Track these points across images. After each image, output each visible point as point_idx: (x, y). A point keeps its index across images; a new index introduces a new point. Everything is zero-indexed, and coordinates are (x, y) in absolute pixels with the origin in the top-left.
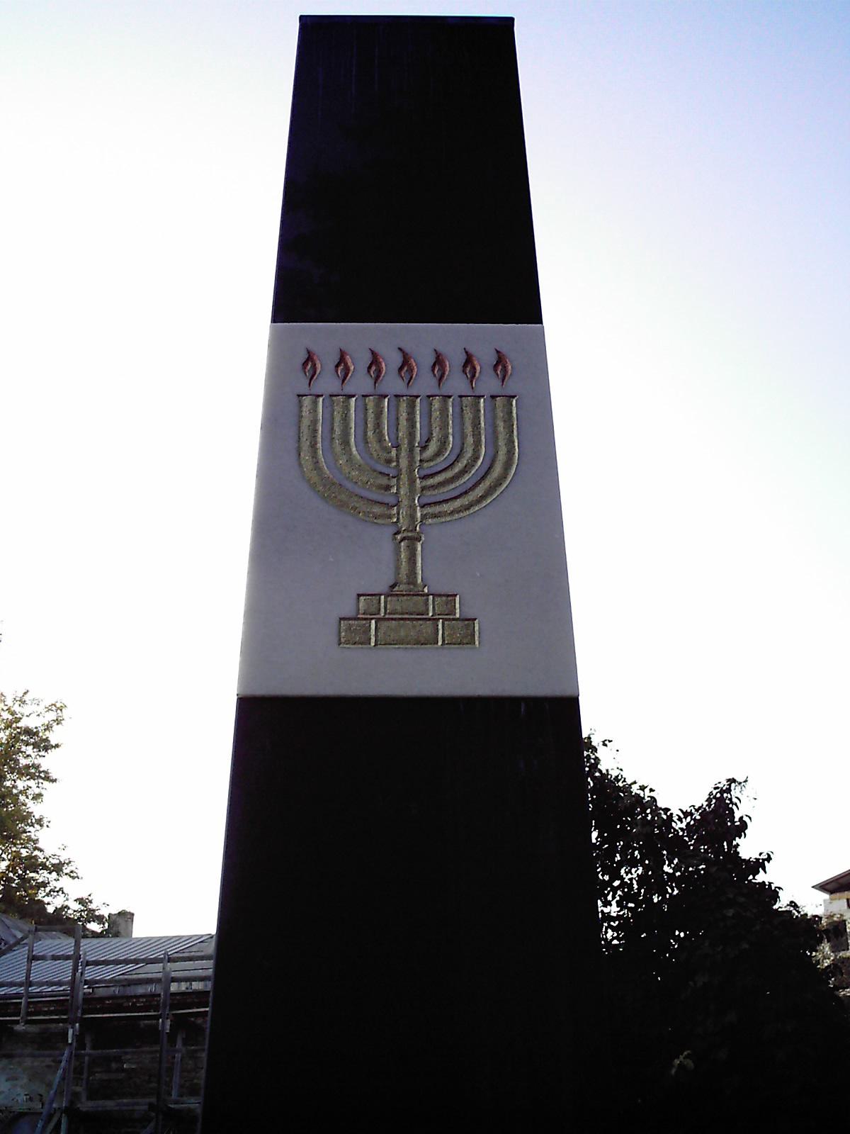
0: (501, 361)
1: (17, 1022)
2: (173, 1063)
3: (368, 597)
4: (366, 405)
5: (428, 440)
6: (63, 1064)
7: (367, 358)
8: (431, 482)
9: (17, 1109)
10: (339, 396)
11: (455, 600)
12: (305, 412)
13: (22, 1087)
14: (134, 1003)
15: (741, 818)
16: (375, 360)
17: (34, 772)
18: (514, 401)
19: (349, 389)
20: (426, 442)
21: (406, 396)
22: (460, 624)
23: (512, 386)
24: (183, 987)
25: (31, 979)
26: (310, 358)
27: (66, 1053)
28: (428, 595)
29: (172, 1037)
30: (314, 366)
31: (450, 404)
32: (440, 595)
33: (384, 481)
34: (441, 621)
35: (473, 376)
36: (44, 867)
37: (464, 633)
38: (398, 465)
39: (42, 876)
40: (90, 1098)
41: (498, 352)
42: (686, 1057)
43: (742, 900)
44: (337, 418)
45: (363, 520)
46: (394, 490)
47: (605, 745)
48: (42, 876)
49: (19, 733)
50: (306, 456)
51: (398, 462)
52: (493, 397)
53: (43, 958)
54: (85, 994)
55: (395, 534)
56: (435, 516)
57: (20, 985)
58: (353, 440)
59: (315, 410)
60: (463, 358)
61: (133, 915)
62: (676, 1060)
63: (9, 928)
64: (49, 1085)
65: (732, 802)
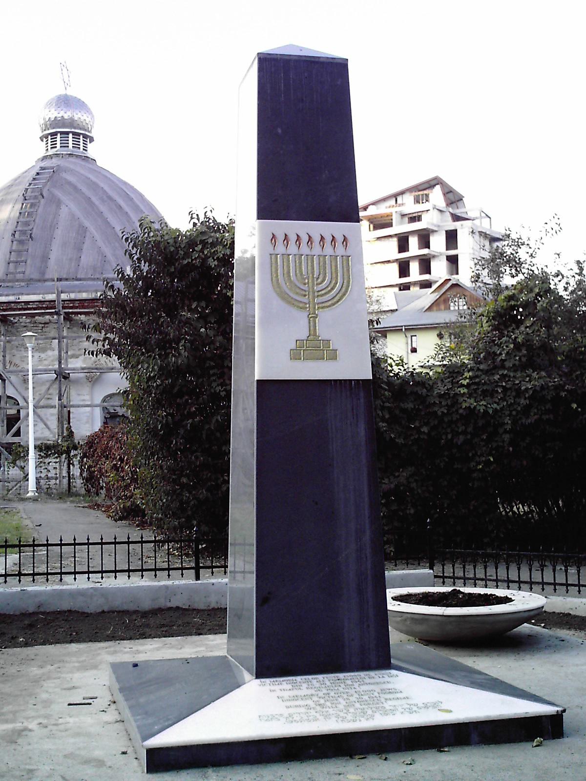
30: (275, 241)
33: (304, 293)
37: (333, 356)
46: (307, 297)
52: (342, 256)
56: (323, 308)
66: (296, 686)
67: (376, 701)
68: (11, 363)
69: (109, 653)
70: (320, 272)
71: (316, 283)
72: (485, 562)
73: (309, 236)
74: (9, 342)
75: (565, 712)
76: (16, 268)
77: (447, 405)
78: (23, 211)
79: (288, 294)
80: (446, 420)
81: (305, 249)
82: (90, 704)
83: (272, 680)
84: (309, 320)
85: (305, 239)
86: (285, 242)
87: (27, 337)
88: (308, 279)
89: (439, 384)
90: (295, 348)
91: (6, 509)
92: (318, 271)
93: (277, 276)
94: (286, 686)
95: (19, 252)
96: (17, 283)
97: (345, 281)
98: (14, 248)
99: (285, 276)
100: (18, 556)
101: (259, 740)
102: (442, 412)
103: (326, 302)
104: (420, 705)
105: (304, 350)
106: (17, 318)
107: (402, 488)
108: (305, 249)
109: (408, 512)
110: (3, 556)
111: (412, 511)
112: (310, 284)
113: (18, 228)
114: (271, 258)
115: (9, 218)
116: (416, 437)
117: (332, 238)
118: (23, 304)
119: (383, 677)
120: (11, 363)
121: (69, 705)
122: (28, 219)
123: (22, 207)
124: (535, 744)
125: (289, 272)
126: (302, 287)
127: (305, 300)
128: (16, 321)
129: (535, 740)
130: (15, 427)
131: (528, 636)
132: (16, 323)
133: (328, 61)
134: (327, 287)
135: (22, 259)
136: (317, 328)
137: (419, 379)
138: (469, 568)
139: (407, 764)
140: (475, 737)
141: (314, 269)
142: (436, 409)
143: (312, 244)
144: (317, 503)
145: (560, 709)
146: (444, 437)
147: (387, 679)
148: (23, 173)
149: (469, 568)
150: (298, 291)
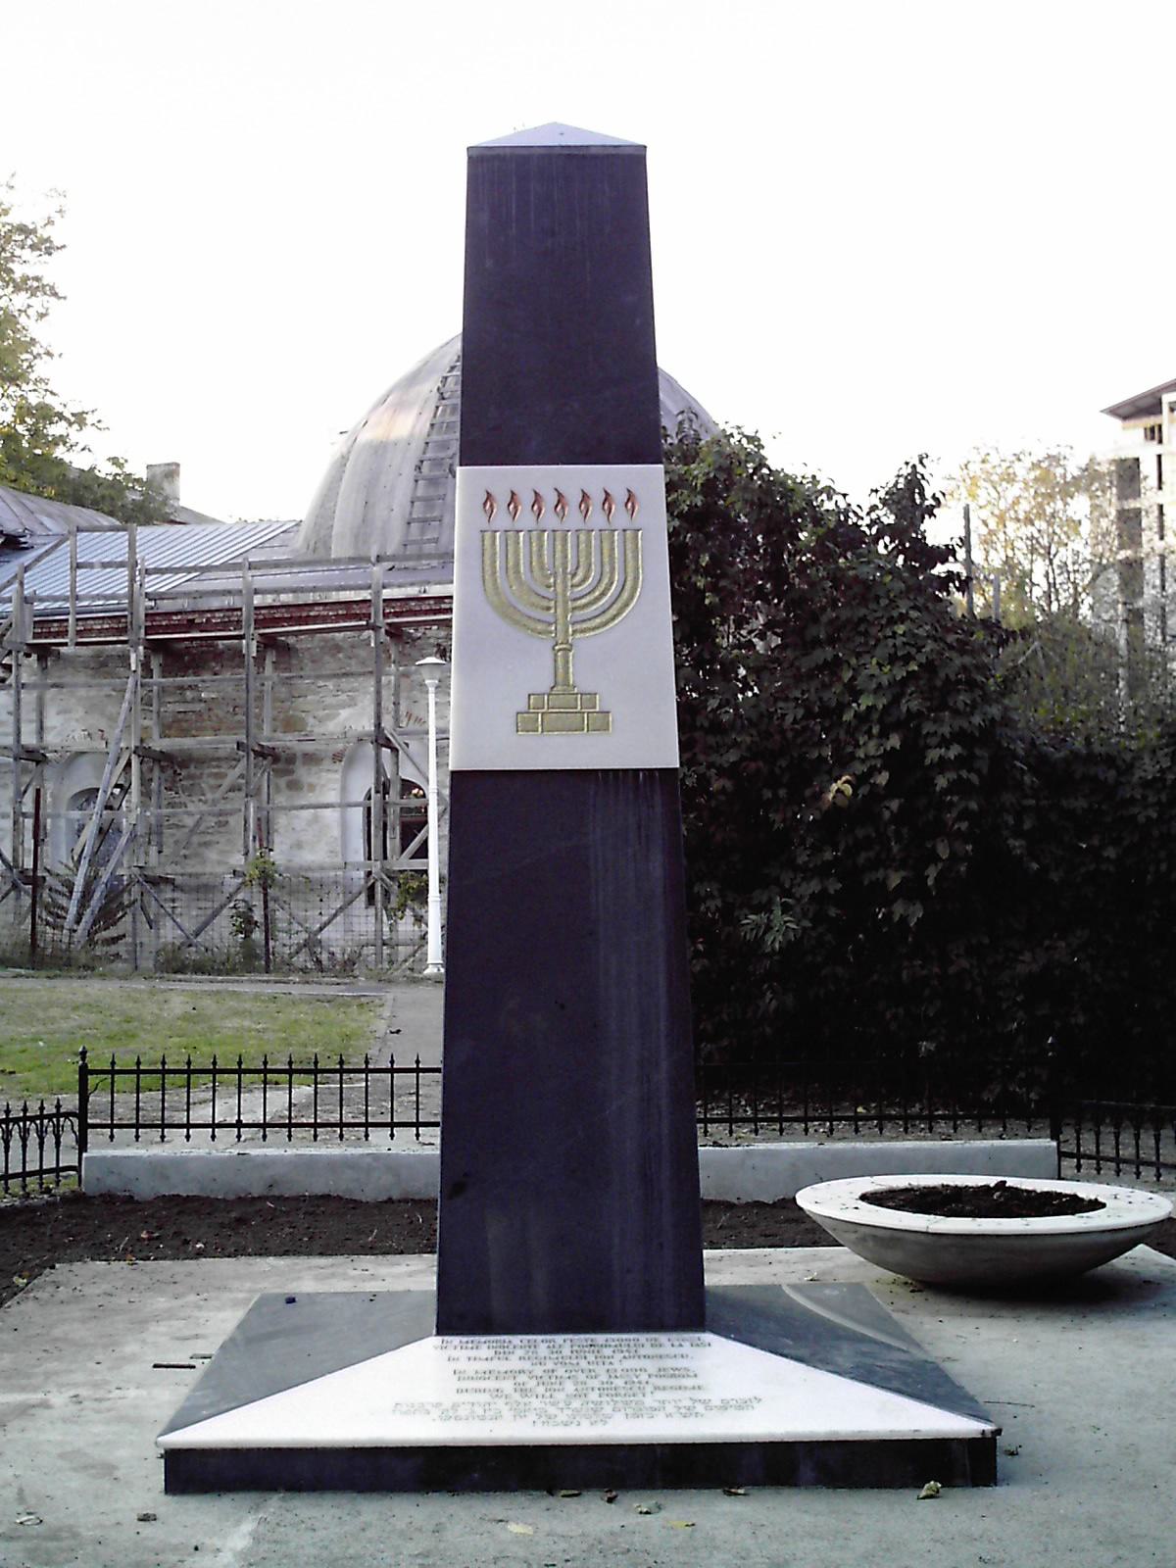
0: (631, 497)
1: (66, 644)
2: (261, 692)
5: (577, 568)
6: (128, 695)
8: (579, 603)
9: (75, 748)
12: (487, 542)
13: (77, 720)
14: (208, 620)
17: (31, 286)
24: (269, 600)
25: (26, 592)
27: (131, 681)
29: (260, 661)
30: (491, 506)
33: (545, 603)
36: (61, 416)
37: (601, 723)
39: (56, 429)
40: (163, 735)
41: (629, 491)
42: (845, 782)
43: (914, 614)
46: (552, 611)
49: (10, 231)
52: (624, 530)
53: (91, 566)
54: (146, 609)
56: (583, 631)
57: (66, 599)
61: (178, 465)
64: (113, 719)
65: (923, 478)
66: (503, 1354)
67: (635, 1390)
68: (409, 716)
69: (317, 1278)
70: (578, 562)
71: (569, 584)
72: (1137, 1128)
73: (560, 495)
74: (406, 675)
75: (1000, 1434)
76: (423, 532)
77: (1159, 803)
78: (436, 421)
79: (515, 608)
80: (1156, 833)
81: (550, 519)
82: (193, 1367)
83: (464, 1339)
84: (556, 655)
85: (550, 499)
86: (512, 506)
87: (426, 669)
88: (555, 577)
89: (1147, 760)
90: (526, 709)
91: (362, 999)
92: (575, 560)
93: (494, 573)
94: (485, 1352)
95: (428, 501)
96: (424, 562)
97: (629, 578)
98: (420, 493)
99: (511, 572)
100: (311, 1090)
101: (372, 1448)
102: (1149, 818)
103: (590, 619)
104: (716, 1402)
105: (543, 714)
106: (422, 629)
107: (1057, 972)
108: (550, 519)
109: (1073, 1021)
110: (283, 1089)
111: (1081, 1020)
112: (559, 588)
113: (429, 455)
114: (483, 537)
115: (412, 435)
116: (1092, 867)
117: (604, 496)
118: (432, 602)
119: (681, 1345)
120: (409, 716)
121: (155, 1366)
122: (446, 437)
123: (435, 414)
124: (923, 1493)
125: (517, 564)
126: (543, 591)
127: (548, 616)
128: (419, 635)
129: (927, 1486)
130: (417, 839)
131: (1145, 1282)
132: (419, 638)
133: (606, 152)
134: (593, 591)
135: (434, 515)
136: (571, 670)
137: (1103, 750)
138: (1147, 1140)
139: (641, 1513)
140: (806, 1471)
141: (566, 557)
142: (1135, 810)
143: (563, 508)
144: (562, 1007)
145: (988, 1427)
146: (1152, 869)
147: (687, 1349)
148: (442, 347)
149: (1127, 1138)
150: (535, 599)
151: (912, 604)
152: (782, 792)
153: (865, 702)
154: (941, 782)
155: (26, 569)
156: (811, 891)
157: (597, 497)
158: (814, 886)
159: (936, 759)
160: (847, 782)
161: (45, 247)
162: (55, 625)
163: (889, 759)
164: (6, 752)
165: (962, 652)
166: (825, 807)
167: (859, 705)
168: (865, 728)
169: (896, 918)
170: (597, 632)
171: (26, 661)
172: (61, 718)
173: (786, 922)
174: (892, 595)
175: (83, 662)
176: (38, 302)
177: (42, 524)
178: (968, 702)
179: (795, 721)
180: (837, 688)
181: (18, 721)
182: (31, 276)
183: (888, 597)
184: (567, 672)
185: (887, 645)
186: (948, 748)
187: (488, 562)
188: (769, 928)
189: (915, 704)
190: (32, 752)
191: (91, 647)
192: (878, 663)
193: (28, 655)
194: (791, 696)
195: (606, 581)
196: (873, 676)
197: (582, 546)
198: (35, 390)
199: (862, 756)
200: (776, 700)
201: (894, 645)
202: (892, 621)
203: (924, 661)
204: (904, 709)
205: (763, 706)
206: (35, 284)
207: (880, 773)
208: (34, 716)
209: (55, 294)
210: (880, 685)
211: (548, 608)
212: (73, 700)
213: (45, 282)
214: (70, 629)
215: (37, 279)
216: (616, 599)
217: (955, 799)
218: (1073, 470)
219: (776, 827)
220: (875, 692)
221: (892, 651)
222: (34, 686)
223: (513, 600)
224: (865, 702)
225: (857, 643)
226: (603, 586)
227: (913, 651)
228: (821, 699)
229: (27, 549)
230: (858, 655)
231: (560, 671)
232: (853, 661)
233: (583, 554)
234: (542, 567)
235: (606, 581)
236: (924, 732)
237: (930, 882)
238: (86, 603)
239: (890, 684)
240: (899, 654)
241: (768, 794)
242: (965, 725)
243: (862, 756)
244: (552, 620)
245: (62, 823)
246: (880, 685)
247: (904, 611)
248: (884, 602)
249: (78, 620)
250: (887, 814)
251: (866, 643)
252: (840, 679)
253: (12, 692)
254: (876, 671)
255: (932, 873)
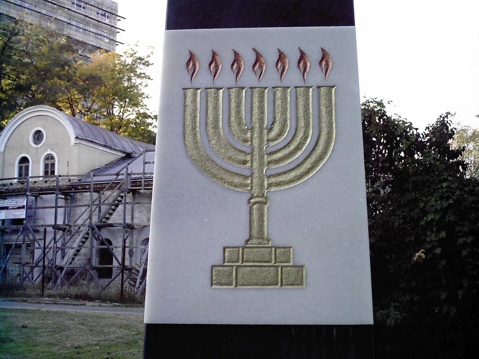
0: (324, 57)
1: (141, 189)
3: (231, 249)
4: (229, 95)
5: (273, 124)
7: (232, 57)
10: (211, 88)
11: (290, 251)
13: (145, 215)
15: (452, 130)
16: (237, 58)
18: (333, 90)
19: (218, 84)
20: (271, 125)
21: (258, 88)
22: (293, 269)
23: (333, 78)
25: (145, 172)
26: (192, 58)
28: (271, 247)
30: (194, 65)
31: (289, 94)
32: (280, 248)
33: (242, 157)
34: (280, 267)
35: (305, 70)
36: (150, 116)
38: (252, 144)
39: (149, 121)
41: (323, 50)
42: (422, 252)
43: (450, 178)
44: (210, 108)
45: (228, 188)
46: (249, 165)
47: (389, 103)
48: (149, 121)
49: (136, 59)
50: (189, 138)
51: (252, 141)
52: (319, 87)
55: (250, 199)
56: (278, 184)
57: (141, 174)
58: (221, 124)
59: (194, 101)
60: (298, 55)
62: (417, 254)
63: (136, 146)
70: (275, 118)
71: (265, 138)
84: (251, 208)
85: (248, 58)
86: (213, 65)
90: (221, 263)
93: (194, 128)
99: (210, 127)
105: (238, 267)
112: (256, 142)
125: (216, 120)
127: (244, 170)
143: (261, 67)
150: (231, 153)
151: (448, 174)
152: (394, 256)
153: (430, 217)
154: (465, 253)
155: (129, 164)
156: (406, 300)
157: (293, 57)
158: (408, 297)
159: (462, 242)
160: (423, 252)
161: (147, 64)
162: (138, 183)
163: (441, 242)
164: (120, 225)
165: (472, 195)
166: (413, 263)
167: (427, 218)
168: (430, 228)
169: (444, 312)
170: (292, 185)
171: (129, 195)
172: (139, 214)
173: (396, 314)
174: (440, 170)
175: (147, 195)
176: (144, 80)
177: (139, 150)
178: (475, 217)
179: (399, 225)
180: (417, 211)
181: (125, 215)
182: (142, 73)
183: (438, 171)
184: (261, 226)
185: (439, 192)
186: (467, 238)
187: (188, 117)
188: (388, 316)
189: (452, 218)
190: (129, 225)
191: (149, 190)
192: (435, 200)
193: (129, 193)
194: (397, 214)
195: (301, 135)
196: (433, 205)
197: (278, 102)
198: (142, 108)
199: (429, 240)
200: (390, 216)
201: (442, 192)
202: (441, 182)
203: (456, 199)
204: (447, 220)
205: (385, 218)
206: (143, 75)
207: (437, 248)
208: (130, 213)
209: (149, 78)
210: (436, 209)
211: (245, 162)
212: (143, 208)
213: (146, 75)
214: (142, 184)
215: (144, 74)
216: (310, 154)
217: (471, 260)
218: (470, 133)
219: (391, 271)
220: (434, 212)
221: (441, 194)
222: (130, 203)
223: (212, 155)
224: (430, 217)
225: (425, 191)
226: (298, 140)
227: (451, 194)
228: (410, 215)
229: (133, 158)
230: (426, 196)
231: (255, 224)
232: (424, 199)
233: (278, 110)
234: (240, 124)
235: (301, 135)
236: (457, 230)
237: (460, 297)
238: (148, 175)
239: (441, 209)
240: (445, 195)
241: (387, 257)
242: (475, 227)
243: (429, 240)
244: (248, 173)
245: (139, 250)
246: (436, 209)
247: (446, 177)
248: (437, 173)
249: (145, 181)
250: (440, 267)
251: (429, 191)
252: (418, 207)
253: (123, 205)
254: (435, 204)
255: (460, 293)
